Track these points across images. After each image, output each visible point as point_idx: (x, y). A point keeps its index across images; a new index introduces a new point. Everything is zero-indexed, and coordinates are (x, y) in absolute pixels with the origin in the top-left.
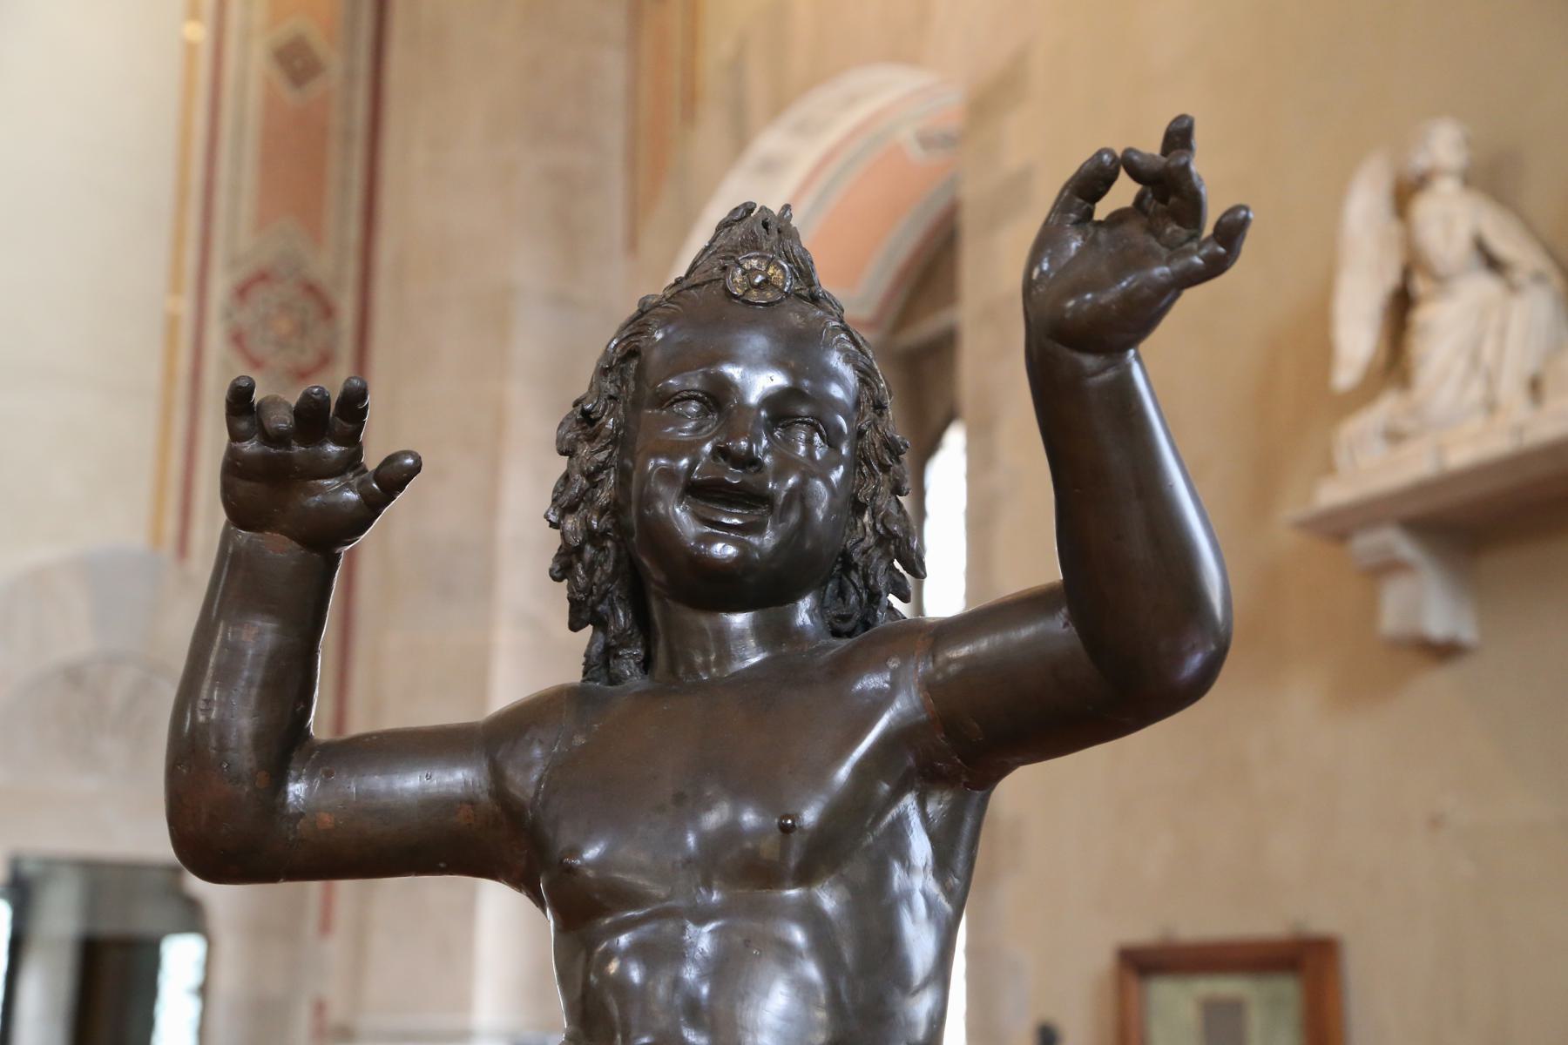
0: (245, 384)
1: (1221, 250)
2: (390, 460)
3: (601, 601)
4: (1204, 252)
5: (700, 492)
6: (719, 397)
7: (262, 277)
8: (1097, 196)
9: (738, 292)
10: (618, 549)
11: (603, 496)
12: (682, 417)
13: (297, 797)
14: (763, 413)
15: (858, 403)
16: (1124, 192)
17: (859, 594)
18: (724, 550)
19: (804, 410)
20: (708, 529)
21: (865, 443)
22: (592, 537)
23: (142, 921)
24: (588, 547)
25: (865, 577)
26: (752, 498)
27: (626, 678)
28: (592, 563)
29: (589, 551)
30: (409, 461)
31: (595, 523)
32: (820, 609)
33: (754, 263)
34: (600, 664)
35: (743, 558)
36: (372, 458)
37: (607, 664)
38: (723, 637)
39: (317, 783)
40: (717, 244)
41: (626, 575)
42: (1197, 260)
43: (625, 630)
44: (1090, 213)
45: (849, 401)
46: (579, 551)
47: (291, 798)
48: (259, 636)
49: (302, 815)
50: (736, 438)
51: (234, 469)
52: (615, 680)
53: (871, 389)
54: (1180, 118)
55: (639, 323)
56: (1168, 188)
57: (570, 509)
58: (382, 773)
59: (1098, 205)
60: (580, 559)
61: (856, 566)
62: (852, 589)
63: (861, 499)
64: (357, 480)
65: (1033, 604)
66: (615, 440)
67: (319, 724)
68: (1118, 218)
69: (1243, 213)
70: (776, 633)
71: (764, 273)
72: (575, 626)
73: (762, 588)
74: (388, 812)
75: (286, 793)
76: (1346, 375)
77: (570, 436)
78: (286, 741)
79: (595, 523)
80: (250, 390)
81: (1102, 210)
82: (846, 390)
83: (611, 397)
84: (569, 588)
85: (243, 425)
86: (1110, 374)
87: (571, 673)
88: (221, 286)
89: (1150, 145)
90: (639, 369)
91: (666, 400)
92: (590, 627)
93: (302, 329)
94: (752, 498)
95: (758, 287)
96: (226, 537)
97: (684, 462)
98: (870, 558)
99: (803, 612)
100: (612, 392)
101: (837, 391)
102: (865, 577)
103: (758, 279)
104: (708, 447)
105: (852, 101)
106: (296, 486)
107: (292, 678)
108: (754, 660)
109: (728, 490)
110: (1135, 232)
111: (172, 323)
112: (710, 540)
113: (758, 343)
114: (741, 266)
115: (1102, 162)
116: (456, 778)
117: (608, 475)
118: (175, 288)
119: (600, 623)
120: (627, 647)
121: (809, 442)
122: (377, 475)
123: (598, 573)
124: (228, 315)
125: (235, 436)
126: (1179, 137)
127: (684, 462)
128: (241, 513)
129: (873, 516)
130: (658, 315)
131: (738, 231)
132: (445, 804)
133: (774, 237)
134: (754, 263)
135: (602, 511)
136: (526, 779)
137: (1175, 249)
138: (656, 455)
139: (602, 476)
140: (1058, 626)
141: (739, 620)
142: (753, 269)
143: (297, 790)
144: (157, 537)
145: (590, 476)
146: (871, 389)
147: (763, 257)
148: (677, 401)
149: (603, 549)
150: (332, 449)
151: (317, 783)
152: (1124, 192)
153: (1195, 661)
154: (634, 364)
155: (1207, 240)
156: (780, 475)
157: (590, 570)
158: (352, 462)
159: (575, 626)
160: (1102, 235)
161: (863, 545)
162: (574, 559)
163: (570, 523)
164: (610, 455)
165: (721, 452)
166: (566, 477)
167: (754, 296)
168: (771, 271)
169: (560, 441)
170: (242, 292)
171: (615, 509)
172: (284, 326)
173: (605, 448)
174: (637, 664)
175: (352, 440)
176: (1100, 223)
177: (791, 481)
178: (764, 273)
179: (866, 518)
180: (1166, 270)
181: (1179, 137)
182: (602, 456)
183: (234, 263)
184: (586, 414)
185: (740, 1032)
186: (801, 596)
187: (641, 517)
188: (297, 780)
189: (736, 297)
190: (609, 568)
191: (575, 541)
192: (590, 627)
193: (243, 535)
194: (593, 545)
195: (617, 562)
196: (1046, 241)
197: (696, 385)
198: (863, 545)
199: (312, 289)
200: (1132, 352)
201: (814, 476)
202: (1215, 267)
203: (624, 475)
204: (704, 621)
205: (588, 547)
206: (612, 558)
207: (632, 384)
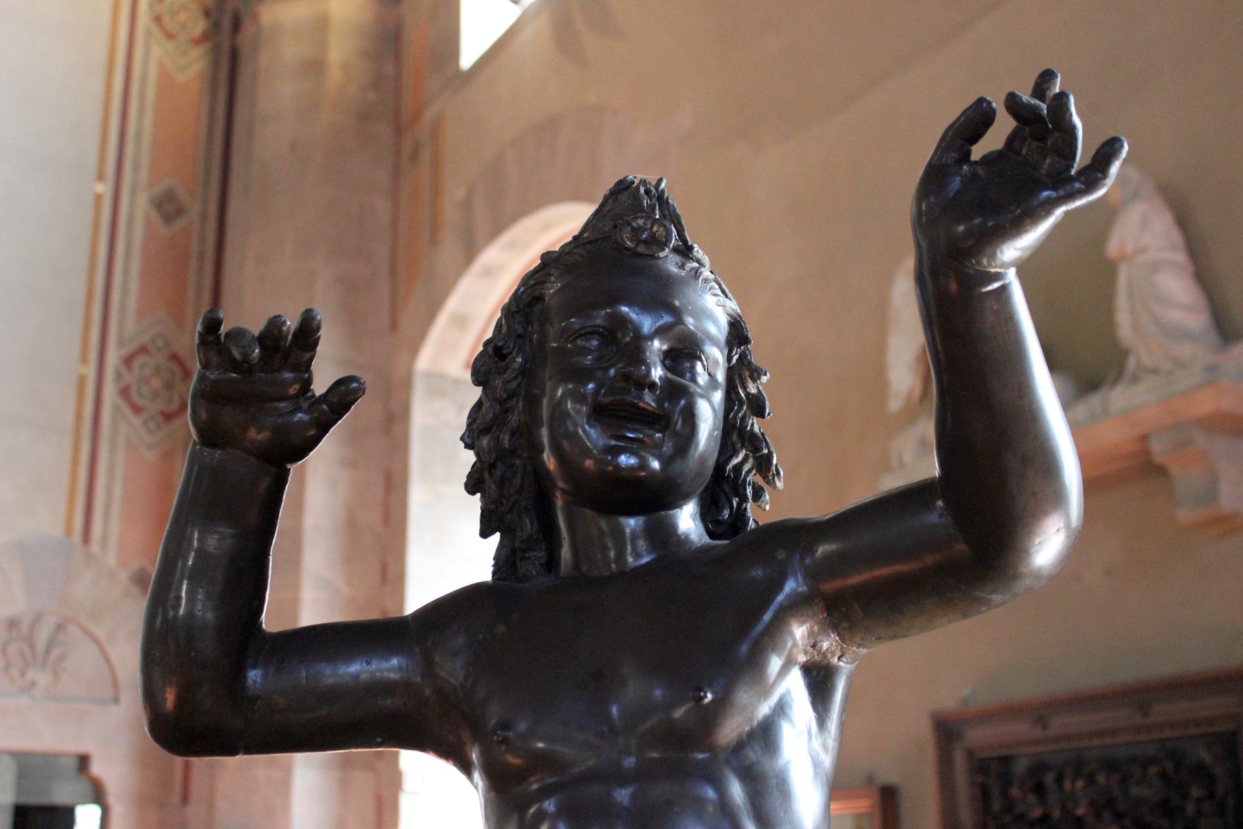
3: (510, 511)
7: (143, 350)
8: (974, 139)
12: (585, 351)
13: (255, 682)
20: (613, 442)
23: (59, 795)
24: (499, 464)
33: (641, 222)
34: (504, 563)
36: (320, 387)
38: (618, 533)
39: (272, 670)
44: (969, 153)
47: (250, 682)
49: (258, 697)
56: (1042, 126)
57: (486, 430)
58: (329, 660)
67: (270, 621)
72: (485, 534)
74: (334, 694)
75: (245, 678)
76: (895, 405)
77: (483, 369)
79: (506, 441)
81: (978, 151)
82: (719, 328)
83: (519, 336)
87: (482, 572)
88: (113, 357)
93: (169, 386)
95: (645, 242)
101: (712, 329)
105: (546, 227)
106: (247, 413)
111: (82, 381)
112: (617, 451)
114: (629, 224)
116: (390, 667)
117: (517, 402)
118: (84, 359)
120: (533, 549)
124: (119, 376)
132: (384, 687)
134: (641, 222)
139: (512, 403)
140: (936, 516)
141: (631, 523)
142: (640, 227)
143: (254, 676)
144: (69, 531)
145: (502, 402)
148: (581, 335)
151: (272, 670)
154: (537, 309)
157: (501, 483)
159: (485, 534)
162: (486, 475)
163: (485, 441)
164: (519, 385)
166: (479, 404)
168: (655, 229)
170: (128, 361)
172: (156, 383)
173: (516, 378)
174: (541, 565)
176: (976, 162)
182: (514, 385)
183: (121, 343)
188: (254, 667)
193: (207, 451)
199: (174, 357)
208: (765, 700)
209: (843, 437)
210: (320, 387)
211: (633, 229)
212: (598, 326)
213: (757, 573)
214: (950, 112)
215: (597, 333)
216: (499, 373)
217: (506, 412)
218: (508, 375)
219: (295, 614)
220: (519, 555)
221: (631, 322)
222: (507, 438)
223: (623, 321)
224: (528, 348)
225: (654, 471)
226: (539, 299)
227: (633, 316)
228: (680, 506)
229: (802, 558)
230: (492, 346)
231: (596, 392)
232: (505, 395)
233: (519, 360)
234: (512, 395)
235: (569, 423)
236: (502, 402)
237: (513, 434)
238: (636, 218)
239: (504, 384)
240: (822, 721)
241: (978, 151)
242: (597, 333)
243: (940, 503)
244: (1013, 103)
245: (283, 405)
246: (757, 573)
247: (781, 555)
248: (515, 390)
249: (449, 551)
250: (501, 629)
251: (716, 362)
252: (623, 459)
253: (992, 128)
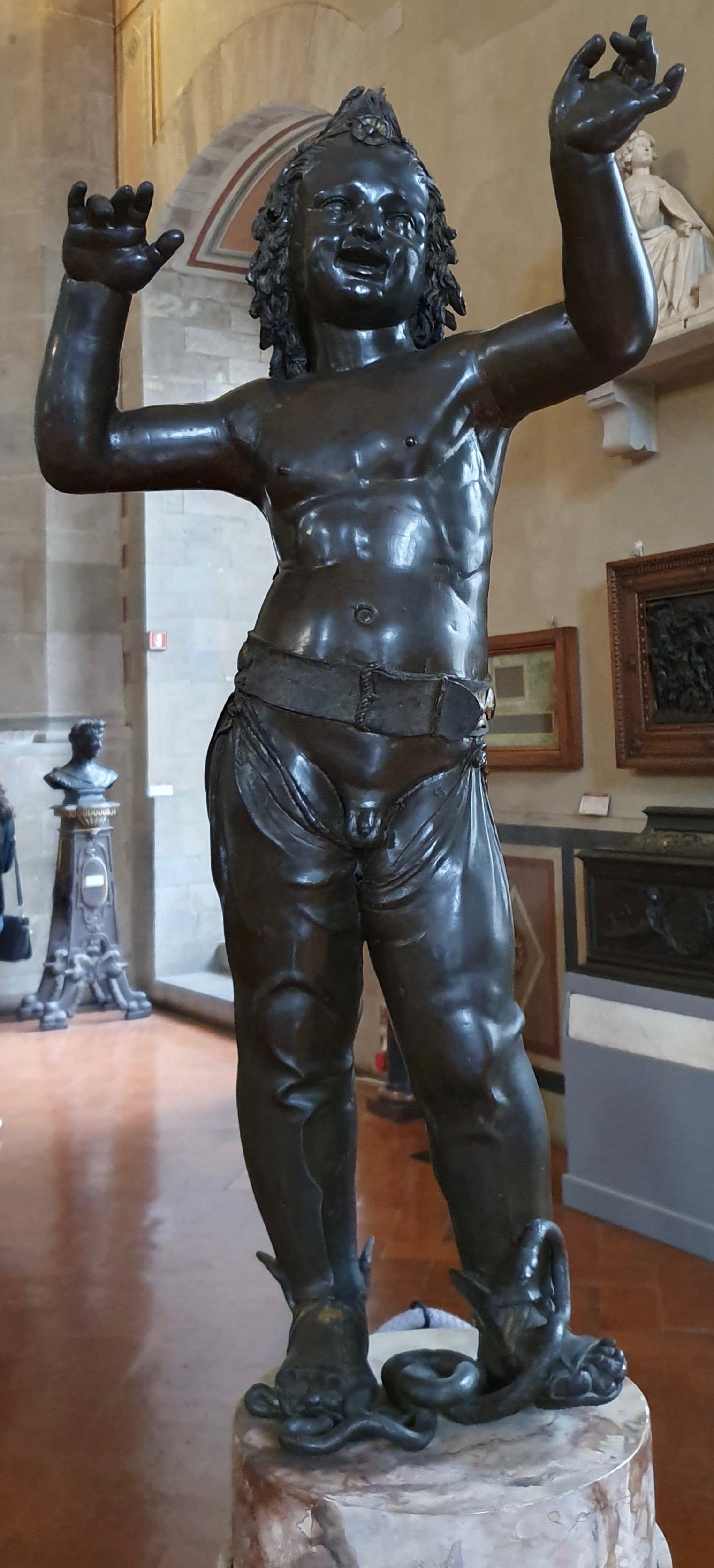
0: (82, 186)
1: (669, 90)
2: (166, 235)
3: (281, 330)
4: (658, 92)
5: (346, 257)
6: (353, 199)
8: (591, 65)
9: (360, 138)
10: (290, 296)
11: (282, 264)
12: (332, 214)
14: (380, 209)
15: (429, 208)
16: (608, 59)
17: (430, 324)
18: (361, 290)
19: (402, 209)
20: (352, 278)
21: (433, 233)
22: (277, 289)
24: (273, 296)
25: (434, 313)
26: (378, 261)
27: (297, 374)
28: (275, 305)
29: (273, 299)
30: (177, 236)
31: (278, 280)
32: (408, 332)
33: (368, 121)
34: (279, 368)
35: (373, 294)
36: (151, 237)
37: (285, 368)
38: (357, 342)
40: (344, 110)
41: (298, 314)
42: (655, 96)
43: (296, 346)
44: (588, 73)
45: (424, 206)
46: (268, 297)
48: (86, 344)
49: (119, 451)
50: (368, 224)
51: (72, 241)
52: (288, 376)
53: (435, 200)
54: (640, 17)
55: (300, 157)
56: (635, 53)
59: (592, 70)
60: (268, 303)
61: (428, 306)
62: (426, 320)
63: (431, 266)
64: (143, 250)
65: (550, 313)
66: (288, 229)
67: (125, 403)
68: (602, 77)
69: (680, 69)
70: (385, 343)
71: (375, 127)
72: (263, 347)
73: (379, 314)
78: (105, 410)
79: (278, 280)
80: (84, 190)
81: (594, 72)
82: (422, 198)
83: (285, 204)
84: (261, 322)
85: (78, 214)
86: (598, 168)
89: (624, 32)
90: (300, 186)
91: (321, 203)
92: (272, 347)
94: (378, 261)
95: (372, 135)
96: (64, 287)
97: (336, 239)
98: (436, 302)
99: (400, 332)
100: (286, 200)
102: (434, 313)
103: (371, 131)
104: (350, 229)
107: (107, 371)
108: (373, 360)
109: (364, 256)
110: (613, 82)
112: (353, 284)
113: (371, 167)
114: (361, 123)
115: (597, 42)
119: (279, 344)
121: (405, 227)
122: (157, 245)
123: (278, 312)
125: (73, 220)
126: (639, 27)
127: (336, 239)
128: (75, 269)
129: (438, 277)
130: (312, 153)
131: (356, 103)
133: (378, 106)
134: (368, 121)
135: (283, 273)
136: (248, 432)
137: (641, 91)
138: (318, 235)
139: (281, 252)
140: (563, 325)
141: (365, 335)
142: (368, 125)
145: (274, 251)
146: (435, 200)
147: (374, 118)
148: (328, 203)
149: (282, 298)
150: (130, 228)
152: (608, 59)
153: (633, 348)
154: (297, 184)
155: (659, 85)
156: (392, 248)
158: (141, 235)
159: (263, 347)
160: (596, 87)
161: (433, 294)
162: (264, 303)
164: (286, 238)
165: (358, 232)
166: (259, 253)
167: (369, 141)
168: (379, 125)
169: (254, 229)
171: (291, 272)
173: (282, 235)
175: (141, 223)
176: (592, 80)
177: (580, 125)
178: (375, 127)
179: (434, 278)
180: (638, 102)
181: (639, 27)
182: (283, 238)
184: (270, 213)
185: (422, 551)
186: (399, 322)
187: (311, 273)
189: (359, 141)
190: (286, 308)
191: (267, 290)
192: (272, 347)
194: (276, 295)
195: (290, 306)
196: (563, 91)
197: (340, 193)
198: (433, 294)
200: (613, 154)
201: (411, 247)
202: (665, 100)
203: (295, 253)
204: (345, 334)
205: (273, 296)
206: (287, 304)
207: (297, 196)
208: (452, 447)
209: (506, 270)
210: (151, 237)
211: (363, 126)
212: (340, 196)
213: (447, 365)
214: (577, 45)
215: (340, 201)
216: (271, 231)
217: (277, 258)
218: (278, 233)
219: (141, 402)
220: (287, 359)
221: (362, 192)
222: (278, 276)
223: (358, 193)
224: (291, 213)
225: (379, 297)
226: (298, 177)
227: (363, 189)
228: (397, 325)
229: (477, 356)
230: (266, 211)
231: (340, 241)
232: (277, 246)
233: (286, 221)
234: (282, 246)
235: (321, 265)
236: (274, 251)
237: (283, 273)
238: (366, 118)
239: (276, 238)
240: (488, 465)
241: (594, 72)
242: (340, 201)
243: (565, 315)
244: (616, 43)
245: (127, 250)
246: (447, 365)
247: (462, 353)
248: (282, 243)
249: (239, 362)
250: (279, 406)
251: (421, 222)
252: (358, 289)
253: (603, 56)
